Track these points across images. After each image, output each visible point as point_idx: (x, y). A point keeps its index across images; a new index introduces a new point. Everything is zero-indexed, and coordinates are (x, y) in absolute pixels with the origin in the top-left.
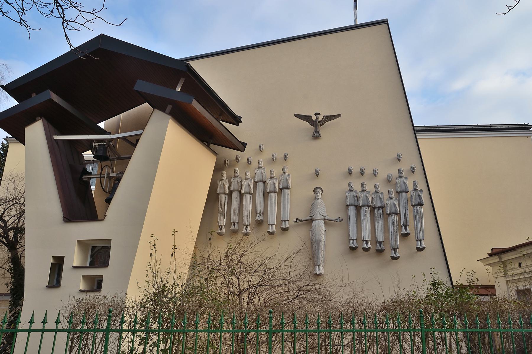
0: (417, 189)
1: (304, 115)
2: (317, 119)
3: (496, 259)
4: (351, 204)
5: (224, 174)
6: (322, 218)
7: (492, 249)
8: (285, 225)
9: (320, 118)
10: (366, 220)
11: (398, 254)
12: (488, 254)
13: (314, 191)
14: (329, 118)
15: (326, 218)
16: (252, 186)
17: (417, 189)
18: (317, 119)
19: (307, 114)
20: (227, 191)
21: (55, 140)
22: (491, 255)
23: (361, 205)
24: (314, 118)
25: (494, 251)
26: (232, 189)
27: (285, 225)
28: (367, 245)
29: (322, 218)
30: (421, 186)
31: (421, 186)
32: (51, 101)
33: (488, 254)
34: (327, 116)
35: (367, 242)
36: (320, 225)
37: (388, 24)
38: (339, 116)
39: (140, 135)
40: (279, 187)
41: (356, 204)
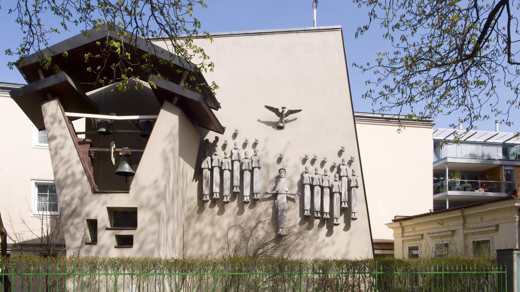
0: (355, 175)
1: (273, 108)
2: (283, 111)
3: (397, 224)
4: (307, 183)
5: (207, 152)
6: (285, 192)
7: (395, 217)
8: (257, 197)
9: (286, 111)
10: (318, 196)
11: (339, 222)
12: (393, 220)
13: (515, 192)
14: (291, 112)
15: (288, 193)
16: (230, 164)
17: (355, 175)
18: (283, 111)
19: (275, 107)
20: (210, 167)
21: (449, 208)
22: (395, 221)
23: (314, 184)
24: (280, 111)
25: (397, 218)
26: (213, 165)
27: (257, 197)
28: (317, 214)
29: (285, 192)
30: (358, 173)
31: (358, 173)
32: (67, 82)
33: (393, 220)
34: (291, 111)
35: (317, 212)
36: (282, 199)
37: (342, 31)
38: (300, 110)
39: (155, 120)
40: (252, 166)
41: (311, 183)
